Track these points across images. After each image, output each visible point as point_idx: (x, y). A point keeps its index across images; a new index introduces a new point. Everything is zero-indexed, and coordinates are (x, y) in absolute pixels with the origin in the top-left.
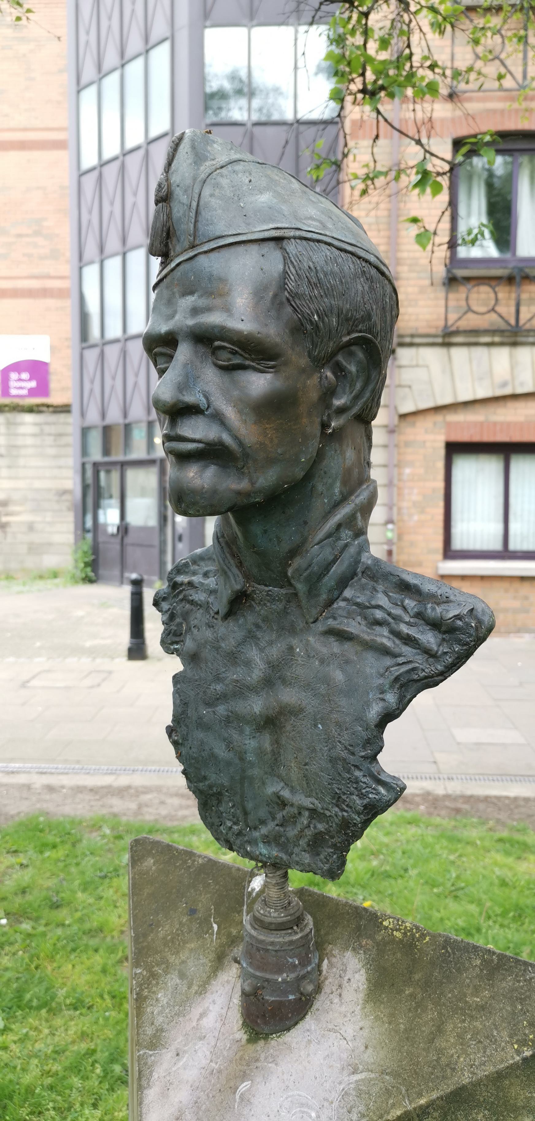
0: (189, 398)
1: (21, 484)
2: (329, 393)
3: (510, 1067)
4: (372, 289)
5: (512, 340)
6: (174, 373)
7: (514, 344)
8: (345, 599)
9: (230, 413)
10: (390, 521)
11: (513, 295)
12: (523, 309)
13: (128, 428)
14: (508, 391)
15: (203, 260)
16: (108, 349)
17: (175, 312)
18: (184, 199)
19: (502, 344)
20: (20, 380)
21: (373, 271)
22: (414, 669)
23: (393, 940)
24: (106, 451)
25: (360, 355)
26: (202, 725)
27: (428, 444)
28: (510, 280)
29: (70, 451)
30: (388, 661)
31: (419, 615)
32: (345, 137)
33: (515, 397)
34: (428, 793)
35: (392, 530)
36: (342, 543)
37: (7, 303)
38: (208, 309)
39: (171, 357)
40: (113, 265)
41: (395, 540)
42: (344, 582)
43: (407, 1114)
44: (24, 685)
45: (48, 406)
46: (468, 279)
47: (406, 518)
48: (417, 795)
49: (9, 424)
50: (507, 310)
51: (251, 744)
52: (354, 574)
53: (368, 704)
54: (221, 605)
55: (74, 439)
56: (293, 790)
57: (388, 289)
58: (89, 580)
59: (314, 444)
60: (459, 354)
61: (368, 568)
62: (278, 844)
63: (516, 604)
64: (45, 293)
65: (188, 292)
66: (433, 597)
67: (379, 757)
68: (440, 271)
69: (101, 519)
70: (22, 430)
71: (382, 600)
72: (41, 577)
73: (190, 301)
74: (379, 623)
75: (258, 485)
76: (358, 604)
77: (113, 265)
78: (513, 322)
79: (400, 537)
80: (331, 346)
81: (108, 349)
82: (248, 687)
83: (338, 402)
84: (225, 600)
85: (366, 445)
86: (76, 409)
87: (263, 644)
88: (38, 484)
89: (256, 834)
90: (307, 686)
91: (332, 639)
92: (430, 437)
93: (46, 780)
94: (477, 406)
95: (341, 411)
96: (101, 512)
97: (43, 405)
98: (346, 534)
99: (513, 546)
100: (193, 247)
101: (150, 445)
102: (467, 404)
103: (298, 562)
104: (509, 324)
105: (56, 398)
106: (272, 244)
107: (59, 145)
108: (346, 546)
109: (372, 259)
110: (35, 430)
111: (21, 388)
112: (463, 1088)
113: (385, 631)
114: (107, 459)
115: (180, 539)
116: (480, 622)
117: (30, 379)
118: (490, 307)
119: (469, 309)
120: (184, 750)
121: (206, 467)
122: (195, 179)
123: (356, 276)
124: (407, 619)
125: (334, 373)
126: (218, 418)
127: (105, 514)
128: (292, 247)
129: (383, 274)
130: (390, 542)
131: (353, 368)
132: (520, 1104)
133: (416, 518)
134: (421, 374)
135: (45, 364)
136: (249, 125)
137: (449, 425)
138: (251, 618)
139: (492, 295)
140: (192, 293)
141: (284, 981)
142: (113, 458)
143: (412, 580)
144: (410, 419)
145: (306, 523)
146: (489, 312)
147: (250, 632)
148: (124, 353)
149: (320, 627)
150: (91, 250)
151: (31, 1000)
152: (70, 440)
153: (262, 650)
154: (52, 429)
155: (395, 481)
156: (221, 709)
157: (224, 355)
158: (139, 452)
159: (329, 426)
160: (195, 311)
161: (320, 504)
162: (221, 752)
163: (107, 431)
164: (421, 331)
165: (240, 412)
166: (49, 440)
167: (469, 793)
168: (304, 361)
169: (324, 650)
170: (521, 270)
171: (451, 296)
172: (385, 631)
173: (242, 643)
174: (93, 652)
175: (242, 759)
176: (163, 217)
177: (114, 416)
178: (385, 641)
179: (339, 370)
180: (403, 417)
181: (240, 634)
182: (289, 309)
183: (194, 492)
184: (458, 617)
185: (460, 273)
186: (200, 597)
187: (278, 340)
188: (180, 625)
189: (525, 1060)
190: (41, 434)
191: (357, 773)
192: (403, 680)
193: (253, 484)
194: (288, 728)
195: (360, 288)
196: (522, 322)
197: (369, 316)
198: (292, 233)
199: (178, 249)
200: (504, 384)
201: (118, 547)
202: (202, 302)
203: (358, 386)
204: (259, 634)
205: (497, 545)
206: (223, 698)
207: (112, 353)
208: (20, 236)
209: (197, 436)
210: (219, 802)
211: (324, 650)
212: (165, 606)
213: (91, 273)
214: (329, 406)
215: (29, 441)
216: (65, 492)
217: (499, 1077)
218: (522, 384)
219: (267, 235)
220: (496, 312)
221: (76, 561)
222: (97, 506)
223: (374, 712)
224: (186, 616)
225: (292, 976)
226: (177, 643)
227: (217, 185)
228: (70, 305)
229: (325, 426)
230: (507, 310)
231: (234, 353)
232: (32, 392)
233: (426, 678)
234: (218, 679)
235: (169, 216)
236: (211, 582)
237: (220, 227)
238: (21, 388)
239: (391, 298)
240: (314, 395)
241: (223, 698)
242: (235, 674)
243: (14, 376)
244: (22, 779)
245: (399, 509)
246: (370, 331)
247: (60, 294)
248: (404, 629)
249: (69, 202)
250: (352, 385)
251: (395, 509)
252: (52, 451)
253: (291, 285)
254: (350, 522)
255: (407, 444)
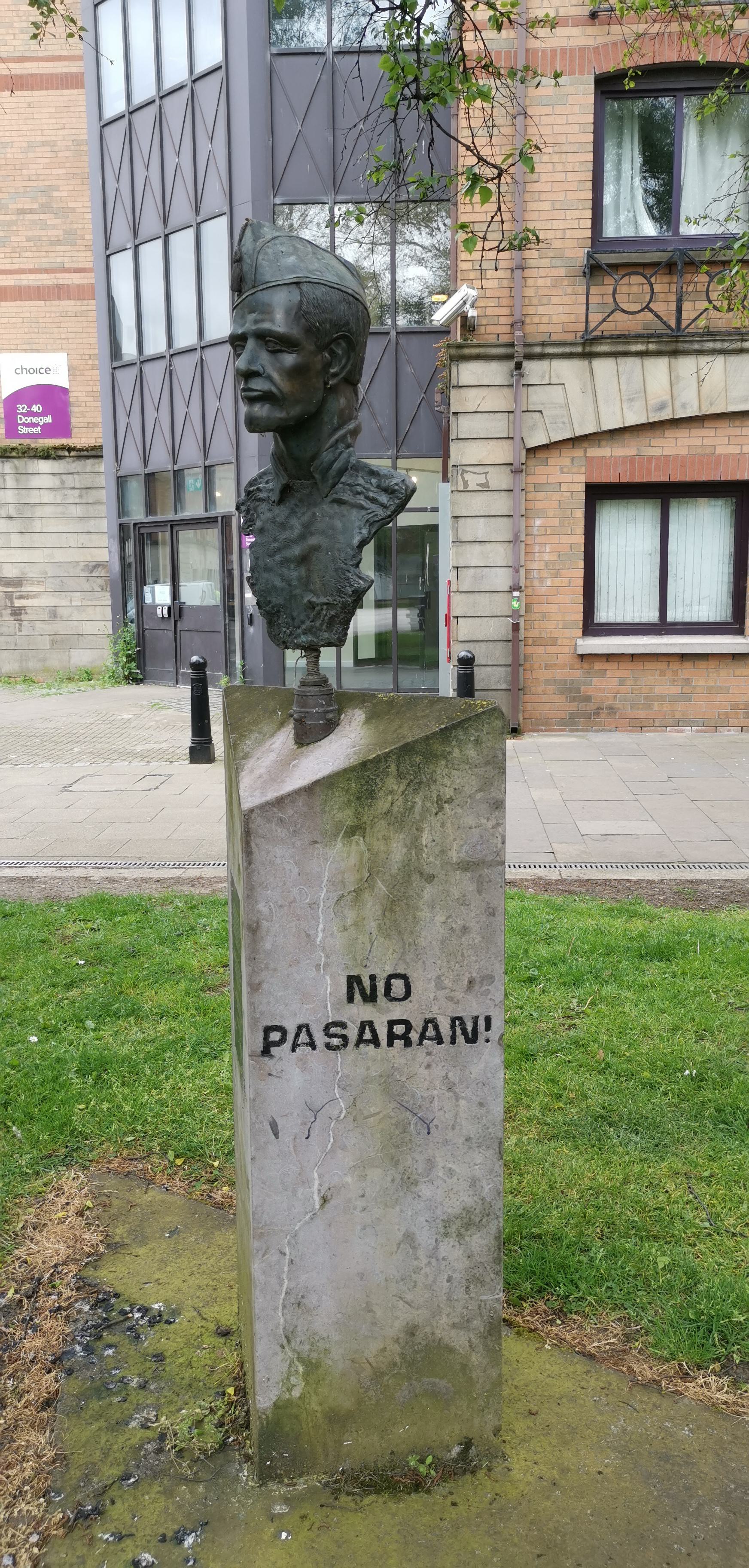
0: (254, 368)
1: (36, 556)
2: (329, 365)
3: (433, 733)
4: (349, 308)
5: (672, 347)
6: (245, 356)
7: (675, 353)
8: (342, 483)
9: (276, 376)
10: (516, 588)
11: (674, 288)
12: (686, 306)
13: (178, 474)
14: (666, 415)
15: (259, 294)
16: (148, 368)
17: (246, 322)
18: (249, 261)
19: (659, 353)
20: (31, 414)
21: (351, 299)
22: (376, 515)
23: (382, 701)
24: (150, 507)
25: (344, 344)
26: (267, 569)
27: (564, 487)
28: (670, 267)
29: (102, 510)
30: (363, 512)
31: (378, 487)
32: (400, 143)
33: (675, 423)
34: (540, 878)
35: (518, 599)
36: (339, 451)
37: (8, 307)
38: (263, 321)
39: (244, 347)
40: (152, 253)
41: (522, 612)
42: (342, 472)
43: (378, 756)
44: (66, 788)
45: (70, 449)
46: (615, 267)
47: (536, 583)
48: (527, 880)
49: (19, 474)
50: (665, 307)
51: (295, 574)
52: (346, 469)
53: (352, 537)
54: (275, 497)
55: (107, 495)
56: (318, 597)
57: (361, 307)
58: (134, 679)
59: (320, 394)
60: (603, 367)
61: (354, 465)
62: (312, 634)
63: (675, 690)
64: (59, 292)
65: (252, 311)
66: (386, 476)
67: (360, 565)
68: (579, 255)
69: (148, 599)
70: (35, 482)
71: (361, 481)
72: (70, 679)
73: (253, 316)
74: (359, 493)
75: (291, 415)
76: (348, 485)
77: (152, 253)
78: (673, 324)
79: (528, 607)
80: (327, 340)
81: (148, 368)
82: (291, 541)
83: (332, 371)
84: (277, 492)
85: (354, 399)
86: (108, 452)
87: (299, 515)
88: (60, 556)
89: (299, 631)
90: (323, 533)
91: (335, 506)
92: (568, 478)
93: (104, 873)
94: (627, 436)
95: (335, 375)
96: (147, 589)
97: (63, 448)
98: (341, 446)
99: (671, 617)
100: (254, 287)
101: (209, 499)
102: (613, 433)
103: (317, 462)
104: (669, 327)
105: (80, 439)
106: (294, 286)
107: (72, 81)
108: (341, 453)
109: (350, 291)
110: (54, 482)
111: (34, 425)
112: (408, 744)
113: (362, 497)
114: (151, 519)
115: (251, 622)
116: (407, 487)
117: (43, 414)
118: (644, 305)
119: (617, 308)
120: (257, 588)
121: (263, 405)
122: (254, 250)
123: (340, 302)
124: (372, 489)
125: (329, 354)
126: (269, 378)
127: (153, 592)
128: (304, 287)
129: (357, 299)
130: (515, 614)
131: (340, 352)
132: (439, 753)
133: (549, 583)
134: (556, 393)
135: (65, 391)
136: (330, 54)
137: (589, 460)
138: (293, 501)
139: (647, 288)
140: (254, 312)
141: (317, 712)
142: (159, 518)
143: (375, 469)
144: (541, 455)
145: (319, 440)
146: (642, 310)
147: (292, 509)
148: (170, 374)
149: (329, 499)
150: (121, 233)
151: (119, 1009)
152: (102, 495)
153: (299, 519)
154: (77, 481)
155: (523, 537)
156: (278, 558)
157: (271, 344)
158: (194, 508)
159: (328, 384)
160: (256, 322)
161: (327, 428)
162: (278, 583)
163: (150, 478)
164: (554, 338)
165: (281, 375)
166: (73, 496)
167: (586, 877)
168: (312, 348)
169: (332, 511)
170: (683, 253)
171: (594, 289)
172: (362, 497)
173: (288, 517)
174: (147, 757)
175: (290, 585)
176: (238, 271)
177: (160, 460)
178: (362, 502)
179: (332, 353)
180: (532, 451)
181: (286, 512)
182: (304, 320)
183: (257, 418)
184: (396, 484)
185: (605, 259)
186: (262, 495)
187: (298, 336)
188: (253, 514)
189: (441, 730)
190: (62, 488)
191: (348, 574)
192: (371, 521)
193: (288, 414)
194: (314, 559)
195: (342, 308)
196: (684, 324)
197: (347, 323)
198: (304, 280)
199: (246, 288)
200: (662, 407)
201: (171, 634)
202: (260, 317)
203: (344, 361)
204: (297, 510)
205: (651, 615)
206: (279, 550)
207: (155, 373)
208: (22, 212)
209: (258, 388)
210: (279, 617)
211: (332, 511)
212: (243, 508)
213: (122, 264)
214: (328, 372)
215: (47, 497)
216: (97, 565)
217: (427, 738)
218: (684, 406)
219: (291, 281)
220: (651, 310)
221: (116, 654)
222: (142, 582)
223: (356, 540)
224: (255, 509)
225: (321, 710)
226: (251, 526)
227: (266, 253)
228: (94, 308)
229: (326, 383)
230: (665, 307)
231: (276, 343)
232: (48, 431)
233: (382, 519)
234: (275, 540)
235: (241, 270)
236: (270, 485)
237: (268, 277)
238: (34, 425)
239: (363, 313)
240: (319, 366)
241: (279, 550)
242: (286, 534)
243: (22, 408)
244: (78, 873)
245: (527, 571)
246: (349, 331)
247: (80, 293)
248: (371, 494)
249: (89, 162)
250: (340, 361)
251: (522, 571)
252: (78, 511)
253: (304, 307)
254: (343, 438)
255: (537, 488)
